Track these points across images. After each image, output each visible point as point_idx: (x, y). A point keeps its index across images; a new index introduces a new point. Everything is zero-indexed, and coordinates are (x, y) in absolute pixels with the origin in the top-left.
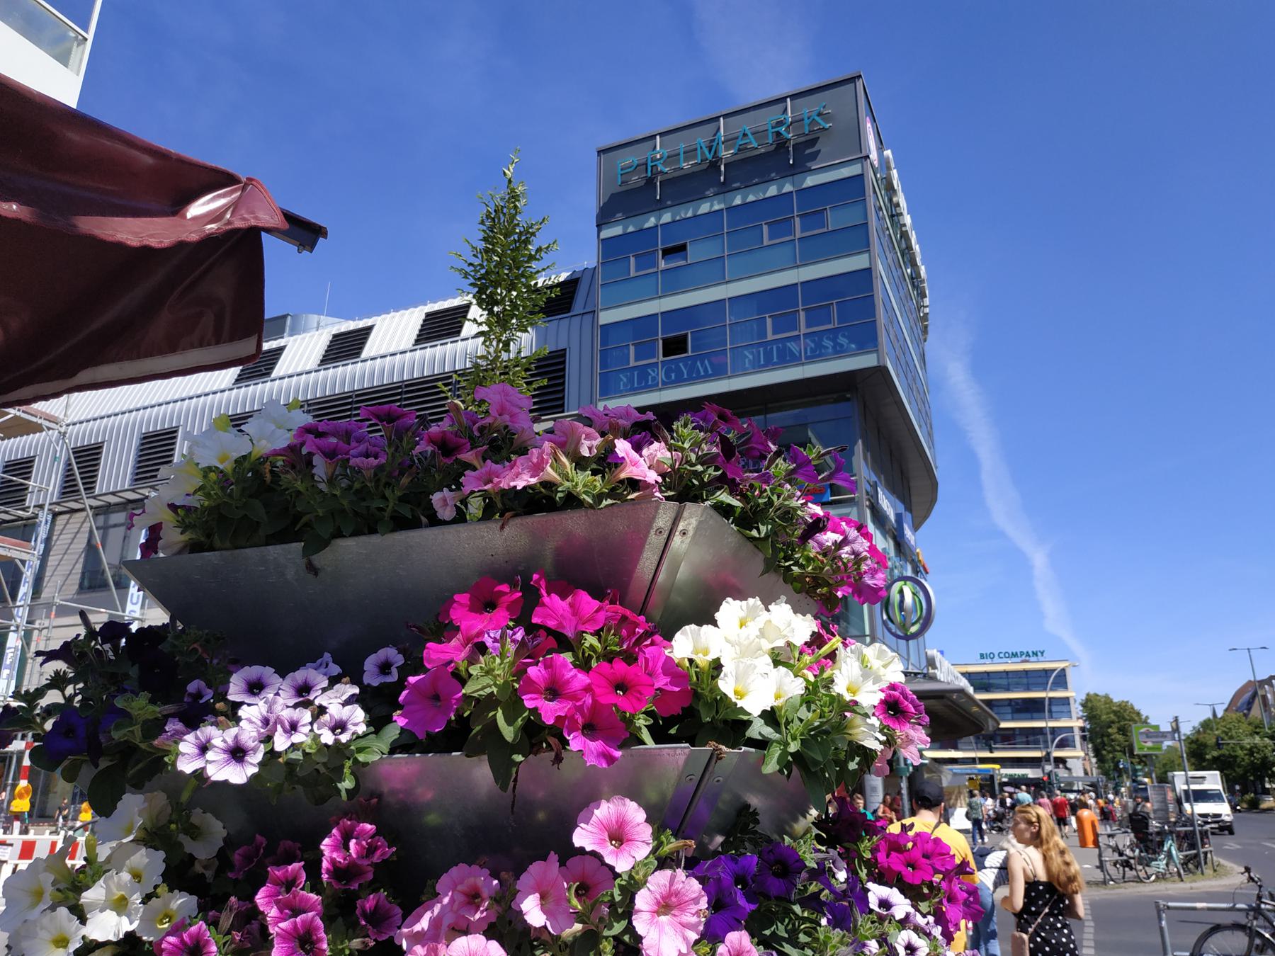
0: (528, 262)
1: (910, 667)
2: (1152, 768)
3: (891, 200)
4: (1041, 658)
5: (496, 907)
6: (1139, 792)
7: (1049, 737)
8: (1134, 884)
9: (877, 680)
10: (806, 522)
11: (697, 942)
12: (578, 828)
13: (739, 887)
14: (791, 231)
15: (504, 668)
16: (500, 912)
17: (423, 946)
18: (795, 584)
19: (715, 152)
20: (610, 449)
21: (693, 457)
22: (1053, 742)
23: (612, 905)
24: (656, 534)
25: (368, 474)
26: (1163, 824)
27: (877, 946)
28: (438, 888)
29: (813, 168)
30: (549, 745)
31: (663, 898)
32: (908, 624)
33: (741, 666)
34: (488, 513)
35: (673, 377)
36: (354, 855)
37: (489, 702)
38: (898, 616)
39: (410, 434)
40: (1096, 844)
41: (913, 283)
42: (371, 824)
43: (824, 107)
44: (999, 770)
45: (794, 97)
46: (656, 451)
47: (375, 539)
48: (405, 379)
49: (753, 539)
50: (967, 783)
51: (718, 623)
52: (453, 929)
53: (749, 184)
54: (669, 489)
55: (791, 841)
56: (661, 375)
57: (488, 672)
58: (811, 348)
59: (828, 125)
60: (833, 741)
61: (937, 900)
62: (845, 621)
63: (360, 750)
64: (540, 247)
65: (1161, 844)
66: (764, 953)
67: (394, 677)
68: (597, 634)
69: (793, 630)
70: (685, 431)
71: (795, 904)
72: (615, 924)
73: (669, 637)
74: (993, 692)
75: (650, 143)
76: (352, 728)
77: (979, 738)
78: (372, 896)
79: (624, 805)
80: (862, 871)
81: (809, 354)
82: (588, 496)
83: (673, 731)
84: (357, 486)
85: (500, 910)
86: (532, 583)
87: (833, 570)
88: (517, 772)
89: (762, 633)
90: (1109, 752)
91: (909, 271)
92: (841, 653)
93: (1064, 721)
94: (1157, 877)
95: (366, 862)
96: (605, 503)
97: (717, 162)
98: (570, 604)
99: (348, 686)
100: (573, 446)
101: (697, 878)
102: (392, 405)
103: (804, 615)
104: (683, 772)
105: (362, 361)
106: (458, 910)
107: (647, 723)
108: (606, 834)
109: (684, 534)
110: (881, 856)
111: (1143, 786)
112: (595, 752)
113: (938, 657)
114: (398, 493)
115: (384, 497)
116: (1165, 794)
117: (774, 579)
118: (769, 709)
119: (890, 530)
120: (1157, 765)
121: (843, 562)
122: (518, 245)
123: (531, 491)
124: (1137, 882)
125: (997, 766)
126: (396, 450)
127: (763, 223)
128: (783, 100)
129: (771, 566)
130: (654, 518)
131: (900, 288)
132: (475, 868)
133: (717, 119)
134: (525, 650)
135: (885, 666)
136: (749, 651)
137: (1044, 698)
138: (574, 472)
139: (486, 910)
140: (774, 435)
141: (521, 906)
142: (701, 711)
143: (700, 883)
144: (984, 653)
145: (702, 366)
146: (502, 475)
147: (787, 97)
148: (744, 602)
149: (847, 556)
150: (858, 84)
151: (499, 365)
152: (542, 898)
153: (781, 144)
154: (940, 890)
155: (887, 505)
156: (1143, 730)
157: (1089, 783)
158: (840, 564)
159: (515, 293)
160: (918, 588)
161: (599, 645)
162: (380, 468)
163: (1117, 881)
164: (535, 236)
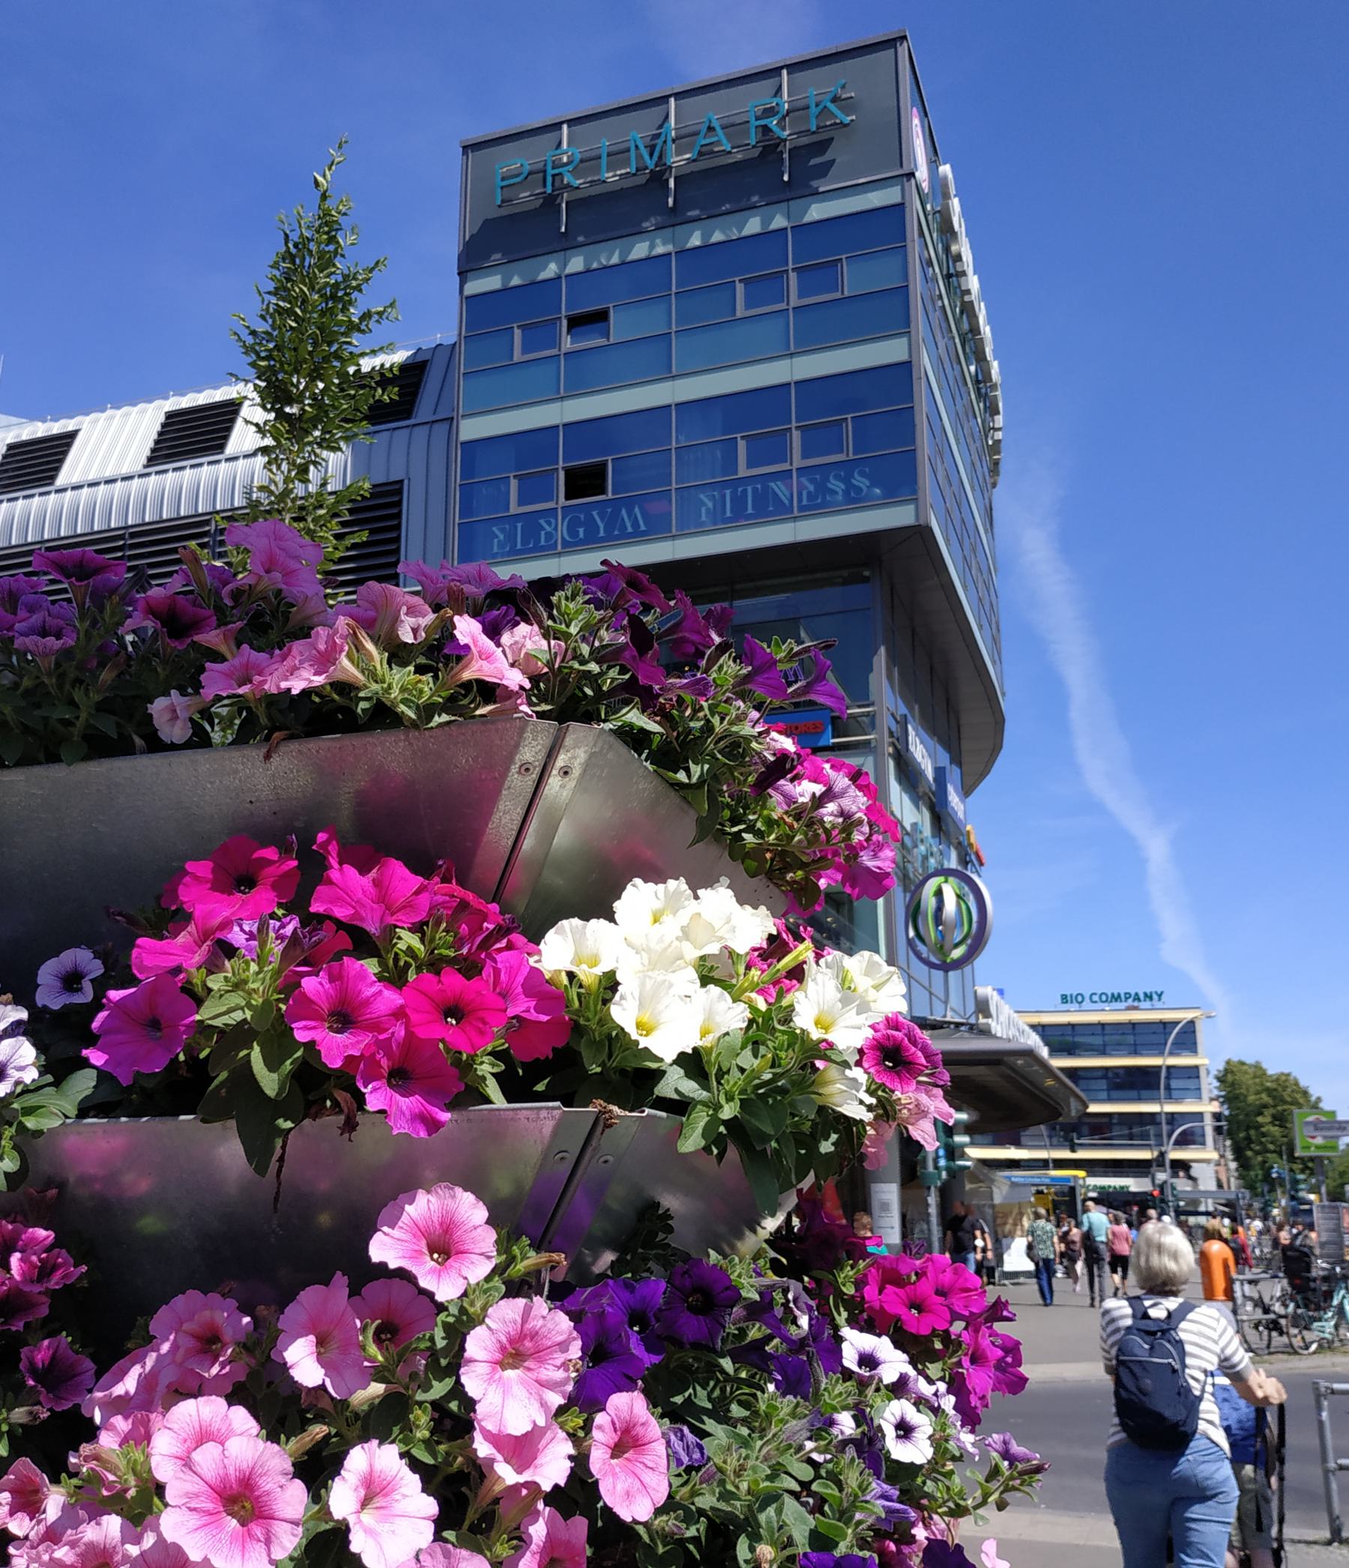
0: (344, 334)
1: (949, 1013)
2: (1321, 1178)
3: (947, 250)
4: (1159, 1005)
5: (246, 1358)
6: (1300, 1214)
7: (1165, 1128)
8: (1285, 1357)
9: (863, 1008)
10: (764, 760)
11: (561, 1411)
12: (379, 1234)
13: (636, 1329)
14: (782, 295)
15: (264, 979)
16: (253, 1365)
17: (126, 1418)
18: (748, 862)
19: (660, 157)
20: (447, 630)
21: (585, 649)
22: (1170, 1136)
23: (433, 1354)
24: (519, 773)
25: (48, 663)
26: (1334, 1264)
27: (853, 1425)
28: (154, 1327)
29: (821, 189)
30: (336, 1104)
31: (511, 1341)
32: (948, 945)
33: (649, 984)
34: (242, 738)
35: (581, 535)
36: (17, 1277)
37: (240, 1035)
38: (932, 934)
39: (116, 599)
40: (1229, 1294)
41: (979, 389)
42: (46, 1229)
43: (843, 87)
44: (1084, 1178)
45: (793, 67)
46: (525, 637)
47: (56, 772)
48: (130, 523)
49: (678, 786)
50: (1032, 1199)
51: (616, 916)
52: (176, 1391)
53: (717, 212)
54: (543, 699)
55: (720, 1257)
56: (562, 531)
57: (238, 985)
58: (809, 493)
59: (849, 118)
60: (792, 1104)
61: (954, 1360)
62: (848, 939)
63: (29, 1111)
64: (369, 311)
65: (1329, 1295)
66: (669, 1429)
67: (87, 995)
68: (418, 928)
69: (733, 930)
70: (571, 605)
71: (723, 1357)
72: (434, 1383)
73: (536, 937)
74: (1079, 1056)
75: (550, 136)
76: (14, 1075)
77: (1054, 1129)
78: (46, 1342)
79: (454, 1197)
80: (840, 1314)
81: (805, 502)
82: (409, 707)
83: (540, 1087)
84: (26, 683)
85: (253, 1362)
86: (314, 847)
87: (807, 840)
88: (283, 1147)
89: (686, 934)
90: (1257, 1153)
91: (973, 368)
92: (810, 968)
93: (1191, 1103)
94: (1320, 1346)
95: (37, 1289)
96: (437, 720)
97: (662, 173)
98: (374, 880)
99: (9, 1007)
100: (386, 626)
101: (567, 1313)
102: (87, 549)
103: (755, 907)
104: (549, 1147)
105: (57, 491)
106: (183, 1362)
107: (496, 1070)
108: (424, 1243)
109: (566, 773)
110: (870, 1292)
111: (1306, 1207)
112: (407, 1113)
113: (994, 999)
114: (96, 697)
115: (72, 703)
116: (1339, 1219)
117: (710, 852)
118: (690, 1051)
119: (926, 794)
120: (1330, 1174)
121: (825, 830)
122: (330, 305)
123: (317, 700)
124: (1289, 1353)
125: (1081, 1173)
126: (94, 623)
127: (737, 279)
128: (776, 71)
129: (709, 830)
130: (517, 746)
131: (958, 398)
132: (215, 1297)
133: (664, 99)
134: (298, 951)
135: (877, 987)
136: (669, 961)
137: (1160, 1067)
138: (386, 666)
139: (230, 1362)
140: (720, 622)
141: (285, 1354)
142: (583, 1054)
143: (570, 1320)
144: (1068, 993)
145: (629, 516)
146: (267, 671)
147: (782, 68)
148: (661, 886)
149: (831, 818)
150: (900, 49)
151: (290, 504)
152: (320, 1343)
153: (770, 148)
154: (960, 1346)
155: (922, 752)
156: (1311, 1119)
157: (1223, 1201)
158: (820, 831)
159: (321, 385)
160: (966, 888)
161: (422, 948)
162: (67, 653)
163: (1260, 1352)
164: (360, 291)
